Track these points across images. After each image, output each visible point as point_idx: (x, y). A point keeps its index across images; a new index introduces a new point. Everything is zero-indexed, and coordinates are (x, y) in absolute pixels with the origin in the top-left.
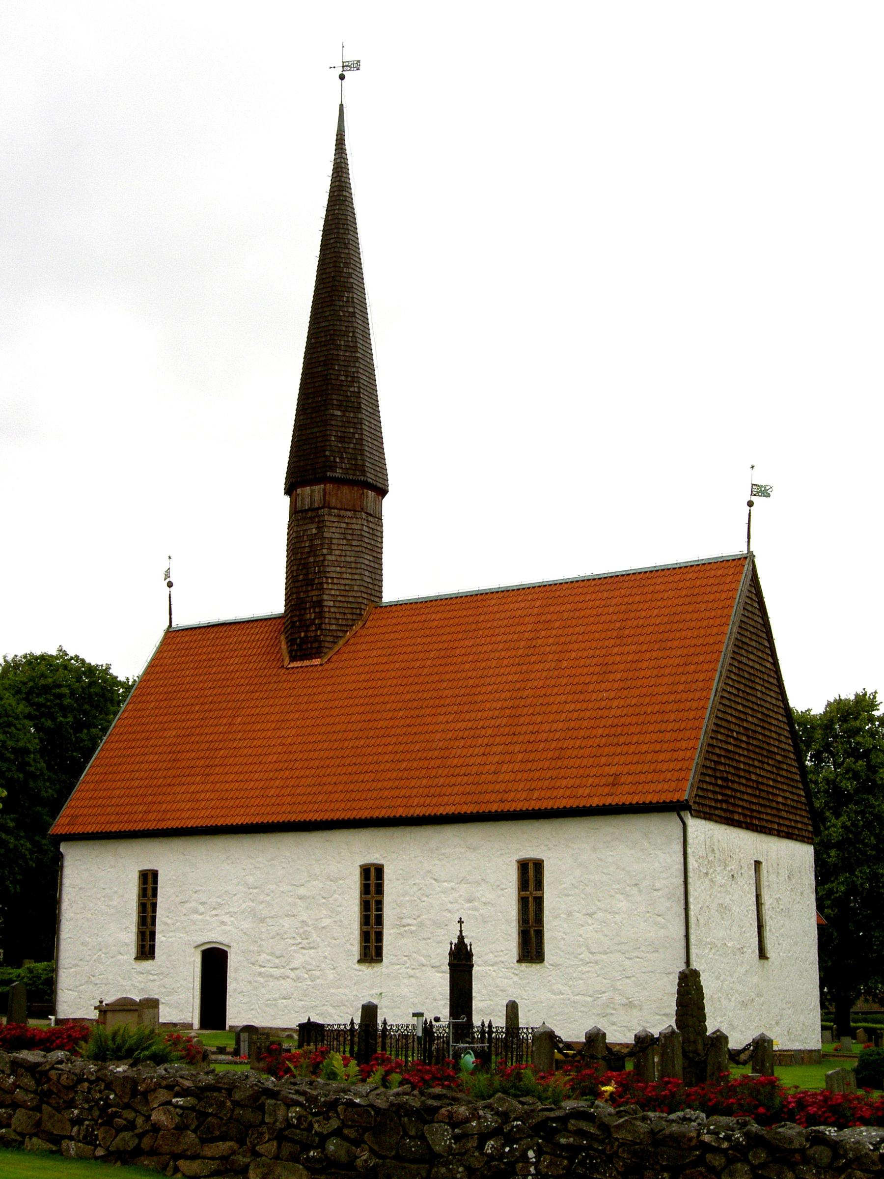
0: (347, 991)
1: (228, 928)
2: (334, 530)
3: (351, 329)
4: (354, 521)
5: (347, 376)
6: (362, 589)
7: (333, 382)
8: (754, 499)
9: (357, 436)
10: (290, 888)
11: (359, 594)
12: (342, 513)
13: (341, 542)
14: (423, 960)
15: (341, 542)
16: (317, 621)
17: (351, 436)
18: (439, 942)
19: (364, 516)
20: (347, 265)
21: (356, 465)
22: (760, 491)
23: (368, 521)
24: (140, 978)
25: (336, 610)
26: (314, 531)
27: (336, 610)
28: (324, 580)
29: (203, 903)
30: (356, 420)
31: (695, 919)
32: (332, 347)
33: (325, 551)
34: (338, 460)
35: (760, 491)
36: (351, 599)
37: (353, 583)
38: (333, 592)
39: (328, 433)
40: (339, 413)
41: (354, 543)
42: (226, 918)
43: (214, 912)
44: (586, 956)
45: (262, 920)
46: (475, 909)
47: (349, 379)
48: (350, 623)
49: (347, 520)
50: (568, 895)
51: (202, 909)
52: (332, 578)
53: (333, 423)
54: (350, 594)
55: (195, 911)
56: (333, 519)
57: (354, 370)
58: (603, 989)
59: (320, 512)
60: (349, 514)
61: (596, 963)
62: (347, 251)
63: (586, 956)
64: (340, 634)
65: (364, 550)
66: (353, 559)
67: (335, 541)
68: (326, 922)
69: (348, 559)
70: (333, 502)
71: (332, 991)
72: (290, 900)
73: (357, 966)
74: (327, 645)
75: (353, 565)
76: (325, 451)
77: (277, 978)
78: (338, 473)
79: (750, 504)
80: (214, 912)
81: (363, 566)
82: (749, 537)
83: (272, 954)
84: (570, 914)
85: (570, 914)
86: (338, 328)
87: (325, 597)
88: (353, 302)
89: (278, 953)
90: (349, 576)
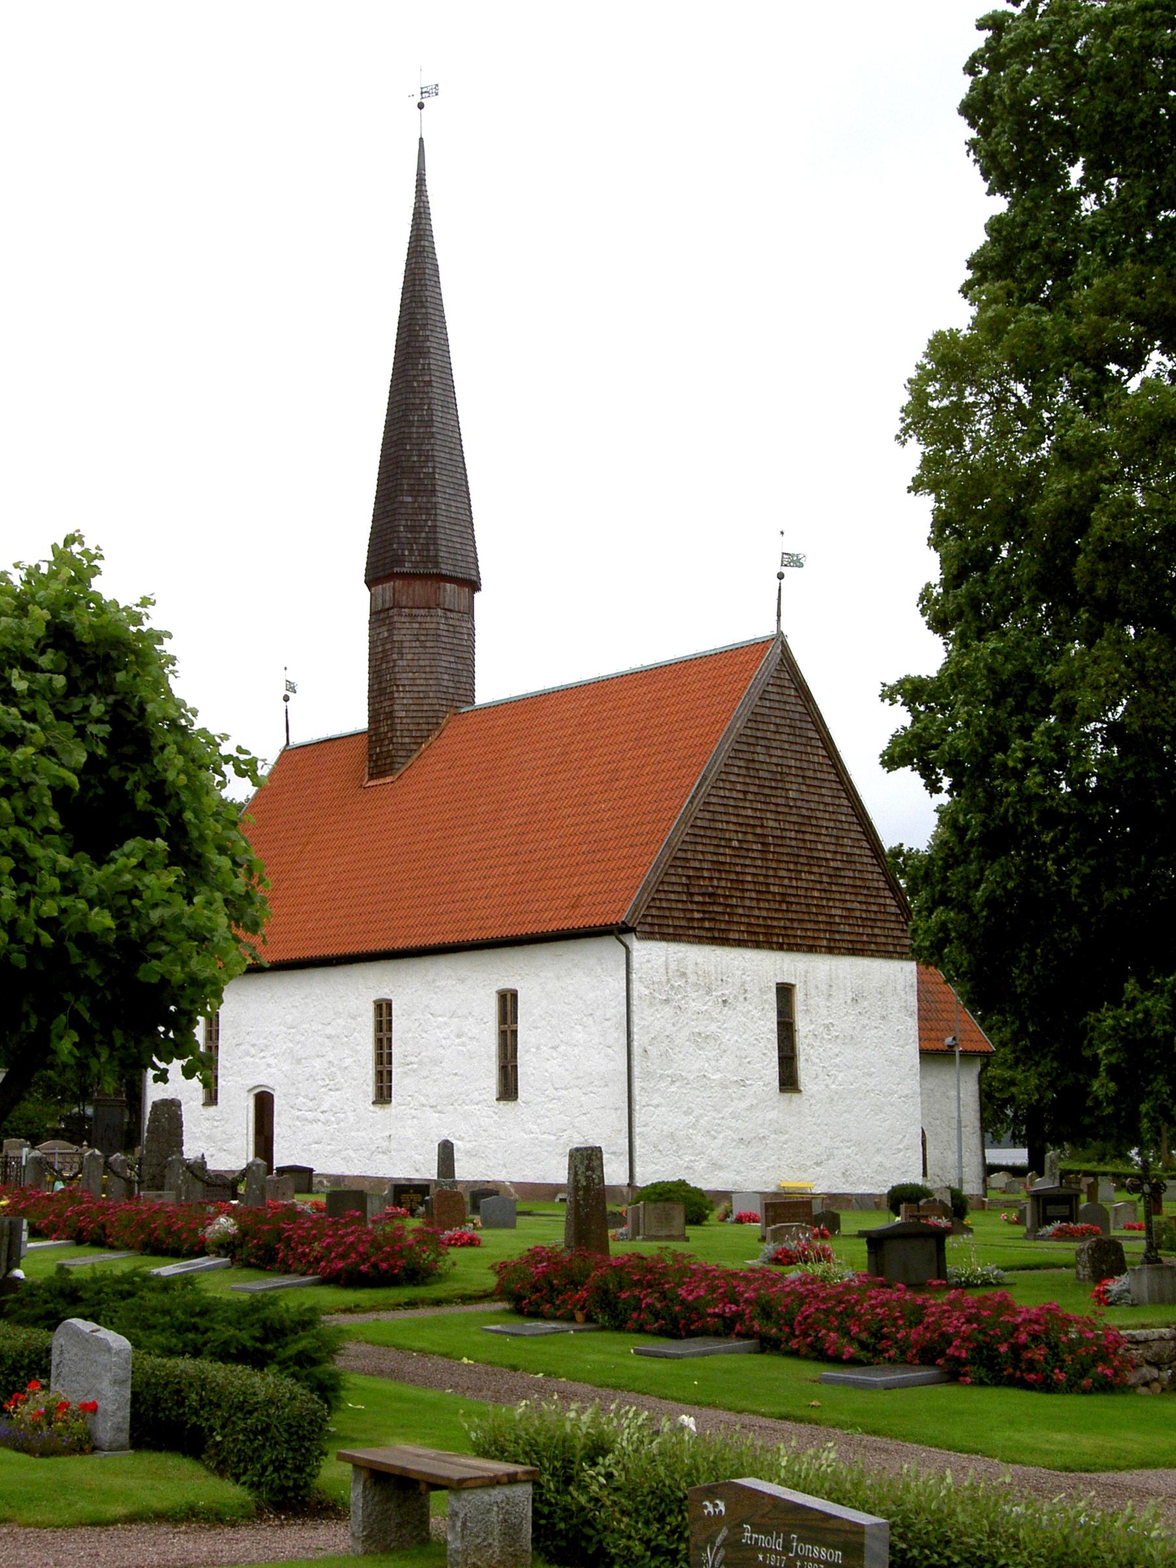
0: (363, 1134)
1: (273, 1070)
2: (403, 632)
3: (426, 401)
4: (428, 619)
5: (420, 456)
6: (439, 695)
7: (404, 464)
8: (784, 570)
9: (430, 523)
10: (320, 1027)
11: (435, 701)
12: (415, 611)
13: (414, 644)
14: (423, 1100)
15: (414, 644)
16: (389, 735)
17: (423, 523)
18: (435, 1081)
19: (440, 612)
20: (424, 327)
21: (428, 556)
22: (792, 560)
23: (446, 618)
24: (207, 1124)
25: (409, 721)
26: (386, 634)
27: (409, 721)
28: (395, 688)
29: (253, 1045)
30: (429, 505)
31: (641, 1050)
32: (404, 424)
33: (395, 656)
34: (406, 553)
35: (792, 560)
36: (425, 708)
37: (428, 689)
38: (405, 701)
39: (396, 523)
40: (410, 499)
41: (428, 644)
42: (271, 1061)
43: (262, 1054)
44: (551, 1092)
45: (299, 1061)
46: (463, 1045)
47: (423, 458)
48: (425, 734)
49: (419, 619)
50: (537, 1028)
51: (253, 1051)
52: (404, 685)
53: (403, 511)
54: (426, 701)
55: (247, 1054)
56: (403, 620)
57: (429, 447)
58: (565, 1127)
59: (391, 612)
60: (422, 612)
61: (559, 1099)
62: (424, 311)
63: (551, 1092)
64: (414, 747)
65: (441, 651)
66: (427, 663)
67: (406, 644)
68: (348, 1061)
69: (422, 663)
70: (404, 601)
71: (353, 1134)
72: (319, 1039)
73: (372, 1108)
74: (399, 760)
75: (428, 669)
76: (392, 544)
77: (311, 1122)
78: (407, 568)
79: (781, 576)
80: (262, 1054)
81: (440, 669)
82: (779, 615)
83: (306, 1097)
84: (538, 1048)
85: (538, 1048)
86: (412, 401)
87: (396, 707)
88: (429, 369)
89: (311, 1095)
90: (422, 682)
